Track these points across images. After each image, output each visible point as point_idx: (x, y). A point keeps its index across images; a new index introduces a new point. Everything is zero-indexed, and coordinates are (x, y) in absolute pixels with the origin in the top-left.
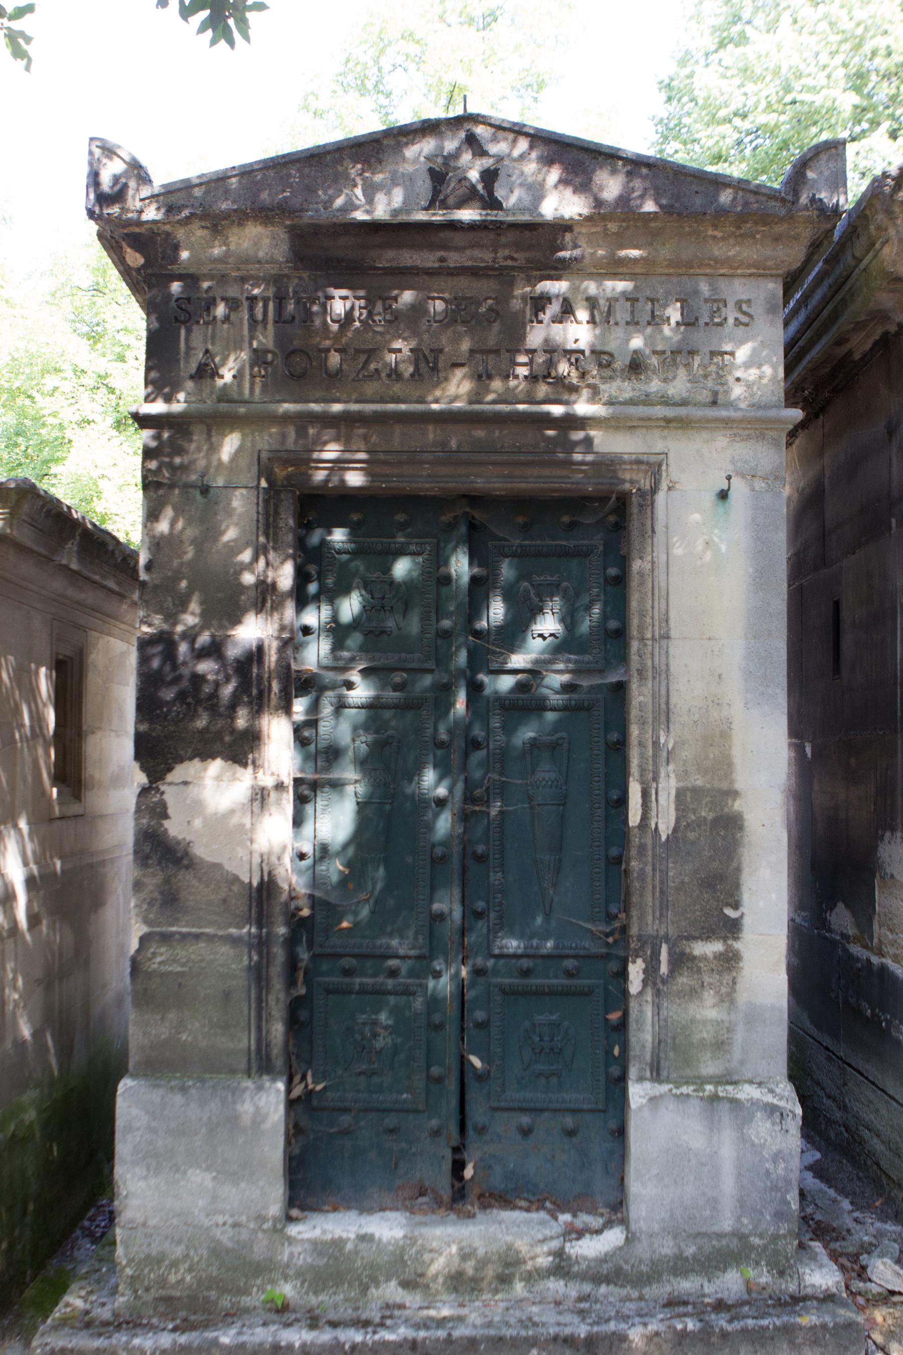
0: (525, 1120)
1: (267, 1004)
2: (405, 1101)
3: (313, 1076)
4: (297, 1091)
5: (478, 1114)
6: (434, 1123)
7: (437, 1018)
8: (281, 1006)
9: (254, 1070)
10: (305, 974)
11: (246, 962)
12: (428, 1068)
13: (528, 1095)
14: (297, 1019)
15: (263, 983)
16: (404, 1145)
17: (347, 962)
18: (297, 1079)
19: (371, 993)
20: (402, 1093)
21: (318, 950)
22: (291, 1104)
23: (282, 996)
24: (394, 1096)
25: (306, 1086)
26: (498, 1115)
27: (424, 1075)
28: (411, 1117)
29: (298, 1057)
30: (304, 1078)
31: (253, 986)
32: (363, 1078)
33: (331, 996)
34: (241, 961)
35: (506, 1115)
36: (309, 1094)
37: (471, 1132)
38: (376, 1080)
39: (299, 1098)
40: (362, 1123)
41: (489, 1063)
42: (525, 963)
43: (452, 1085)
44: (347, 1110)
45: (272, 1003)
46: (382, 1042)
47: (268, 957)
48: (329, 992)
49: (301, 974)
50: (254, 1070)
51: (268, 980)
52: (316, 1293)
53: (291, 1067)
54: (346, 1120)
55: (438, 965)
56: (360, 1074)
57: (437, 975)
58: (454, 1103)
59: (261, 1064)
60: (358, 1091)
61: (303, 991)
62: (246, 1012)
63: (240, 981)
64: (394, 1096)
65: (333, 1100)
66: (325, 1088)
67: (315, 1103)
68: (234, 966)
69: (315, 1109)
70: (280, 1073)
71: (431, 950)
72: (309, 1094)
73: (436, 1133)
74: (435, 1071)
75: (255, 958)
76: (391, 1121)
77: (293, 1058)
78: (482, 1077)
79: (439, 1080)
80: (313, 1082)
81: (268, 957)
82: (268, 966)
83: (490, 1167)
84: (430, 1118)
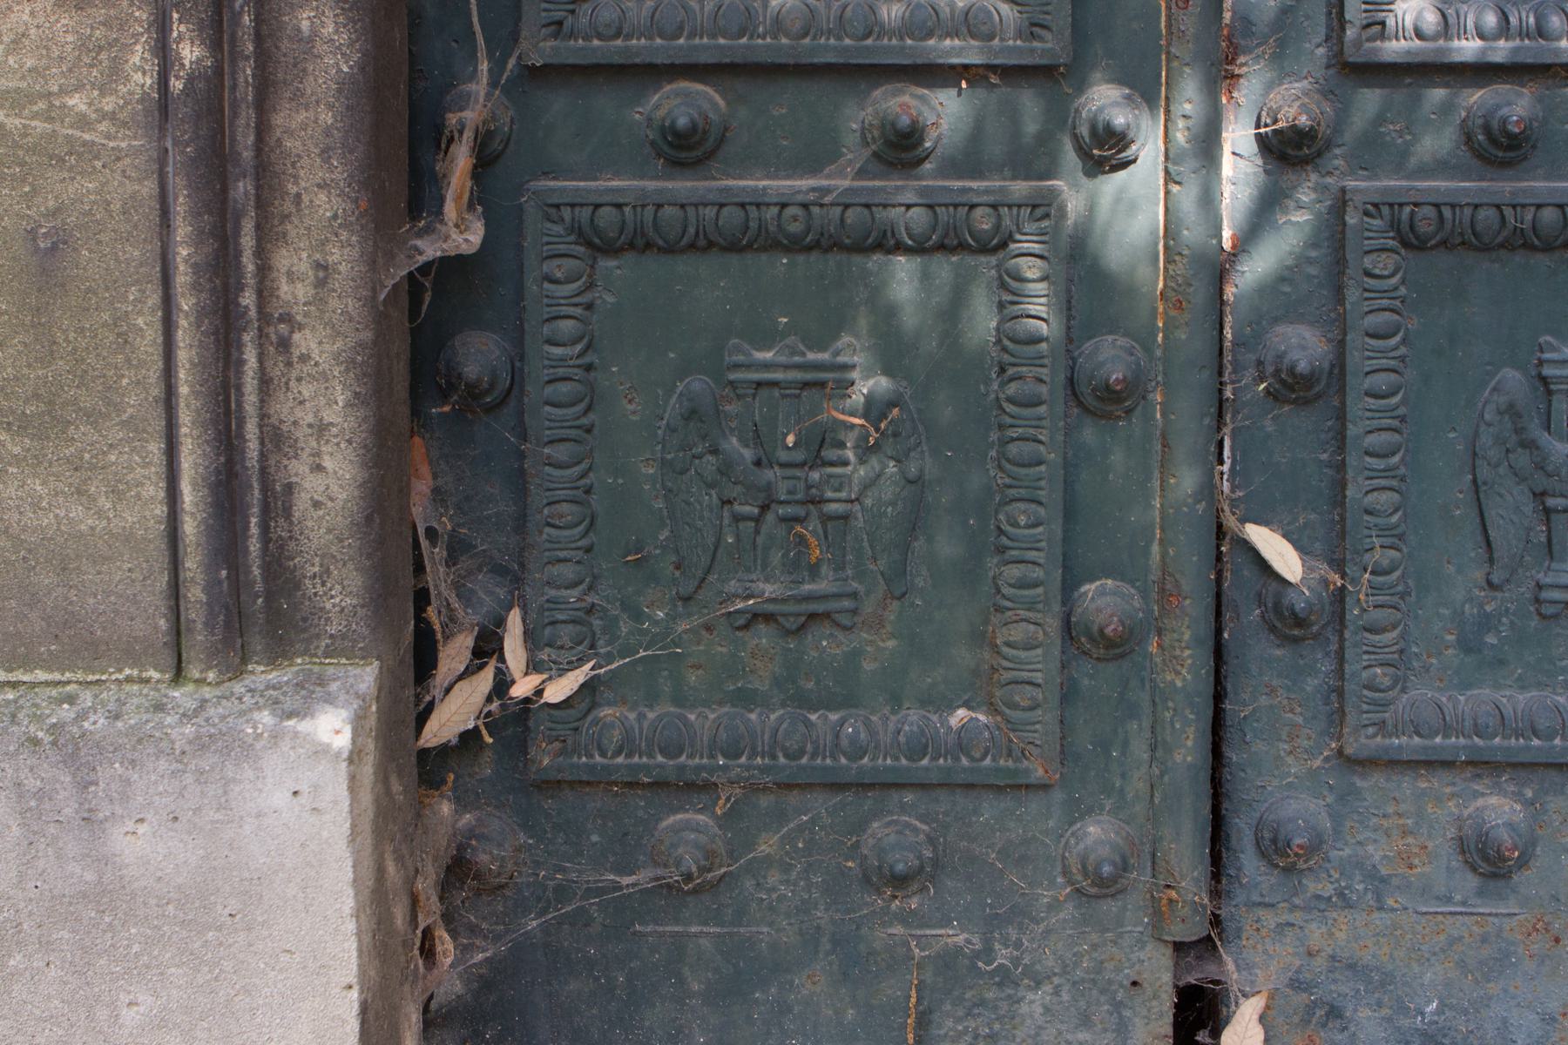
0: (1499, 808)
1: (264, 293)
2: (963, 742)
3: (531, 638)
4: (457, 710)
5: (1285, 781)
6: (1097, 834)
7: (1110, 358)
8: (345, 303)
9: (199, 638)
10: (485, 162)
11: (140, 77)
12: (1069, 586)
13: (1516, 700)
14: (438, 360)
15: (243, 189)
16: (956, 936)
17: (677, 103)
18: (454, 654)
19: (796, 246)
20: (952, 708)
21: (540, 49)
22: (409, 768)
23: (344, 257)
24: (913, 718)
25: (502, 684)
26: (1370, 784)
27: (1053, 624)
28: (988, 810)
29: (456, 549)
30: (487, 647)
31: (181, 205)
32: (763, 637)
33: (607, 264)
34: (116, 71)
35: (1407, 785)
36: (513, 721)
37: (1248, 864)
38: (826, 644)
39: (469, 738)
40: (767, 845)
41: (1339, 565)
42: (1517, 105)
43: (1184, 670)
44: (695, 788)
45: (294, 292)
46: (864, 478)
47: (263, 58)
48: (599, 245)
49: (461, 159)
50: (199, 638)
51: (265, 172)
52: (651, 707)
53: (422, 598)
54: (688, 829)
55: (1104, 100)
56: (756, 617)
57: (1107, 150)
58: (1188, 749)
59: (240, 609)
60: (745, 699)
61: (465, 236)
62: (147, 325)
63: (113, 183)
64: (913, 718)
65: (627, 746)
66: (588, 687)
67: (544, 758)
68: (77, 102)
69: (550, 785)
70: (342, 648)
71: (1079, 35)
72: (513, 721)
73: (1099, 885)
74: (1103, 599)
75: (190, 53)
76: (896, 833)
77: (434, 555)
78: (1288, 621)
79: (1116, 646)
80: (533, 666)
81: (263, 58)
82: (263, 106)
83: (1334, 1012)
84: (1077, 811)
